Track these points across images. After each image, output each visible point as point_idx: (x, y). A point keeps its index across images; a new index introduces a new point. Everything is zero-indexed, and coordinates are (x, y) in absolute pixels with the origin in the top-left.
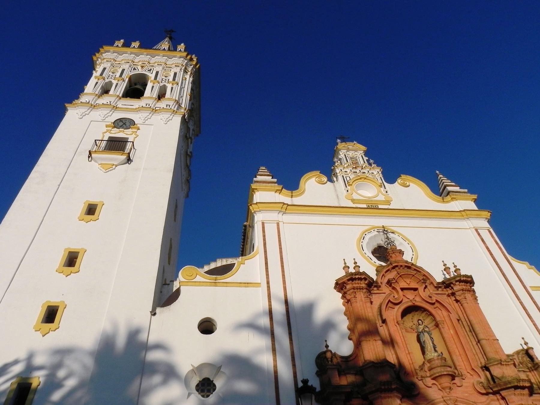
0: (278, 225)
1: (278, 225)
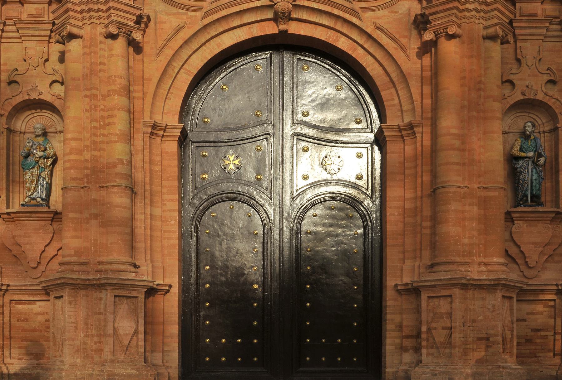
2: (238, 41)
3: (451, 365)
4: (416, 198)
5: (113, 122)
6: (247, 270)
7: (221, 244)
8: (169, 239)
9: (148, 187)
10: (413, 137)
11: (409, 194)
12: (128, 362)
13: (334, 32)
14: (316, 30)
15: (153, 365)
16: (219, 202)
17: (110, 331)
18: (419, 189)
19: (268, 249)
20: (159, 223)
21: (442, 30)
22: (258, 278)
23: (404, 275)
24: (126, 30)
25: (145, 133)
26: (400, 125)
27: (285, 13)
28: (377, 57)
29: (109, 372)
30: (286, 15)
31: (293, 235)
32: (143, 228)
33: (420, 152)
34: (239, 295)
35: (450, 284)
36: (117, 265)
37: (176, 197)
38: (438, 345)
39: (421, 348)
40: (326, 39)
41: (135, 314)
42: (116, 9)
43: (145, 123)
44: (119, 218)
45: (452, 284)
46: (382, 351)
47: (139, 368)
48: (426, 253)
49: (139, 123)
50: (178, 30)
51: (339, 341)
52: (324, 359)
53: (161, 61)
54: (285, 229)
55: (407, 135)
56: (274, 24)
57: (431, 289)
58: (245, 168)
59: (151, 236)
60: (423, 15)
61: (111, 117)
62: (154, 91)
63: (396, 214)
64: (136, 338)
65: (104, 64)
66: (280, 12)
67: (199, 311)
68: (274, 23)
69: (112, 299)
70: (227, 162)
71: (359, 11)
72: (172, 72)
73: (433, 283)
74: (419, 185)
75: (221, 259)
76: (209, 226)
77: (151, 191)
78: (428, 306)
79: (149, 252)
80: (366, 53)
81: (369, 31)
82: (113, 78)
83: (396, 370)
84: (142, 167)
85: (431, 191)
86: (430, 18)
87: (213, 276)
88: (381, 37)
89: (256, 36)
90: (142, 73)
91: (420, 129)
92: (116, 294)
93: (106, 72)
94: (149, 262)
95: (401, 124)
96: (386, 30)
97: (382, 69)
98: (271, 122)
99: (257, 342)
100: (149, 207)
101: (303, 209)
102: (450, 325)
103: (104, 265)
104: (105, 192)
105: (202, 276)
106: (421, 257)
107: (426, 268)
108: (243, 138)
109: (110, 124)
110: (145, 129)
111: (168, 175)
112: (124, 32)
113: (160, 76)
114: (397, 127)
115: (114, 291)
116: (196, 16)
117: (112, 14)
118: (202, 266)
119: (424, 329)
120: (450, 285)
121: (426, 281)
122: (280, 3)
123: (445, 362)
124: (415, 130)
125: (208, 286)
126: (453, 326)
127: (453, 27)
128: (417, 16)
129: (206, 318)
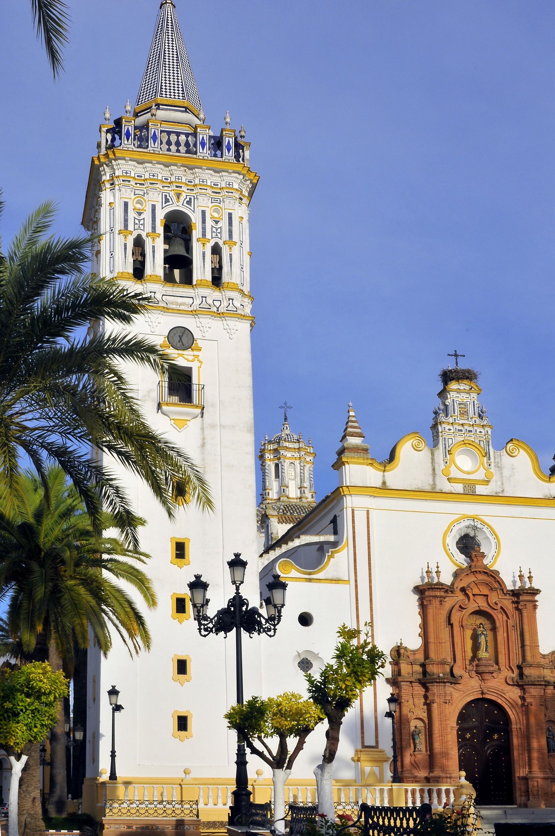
0: (368, 511)
1: (368, 511)
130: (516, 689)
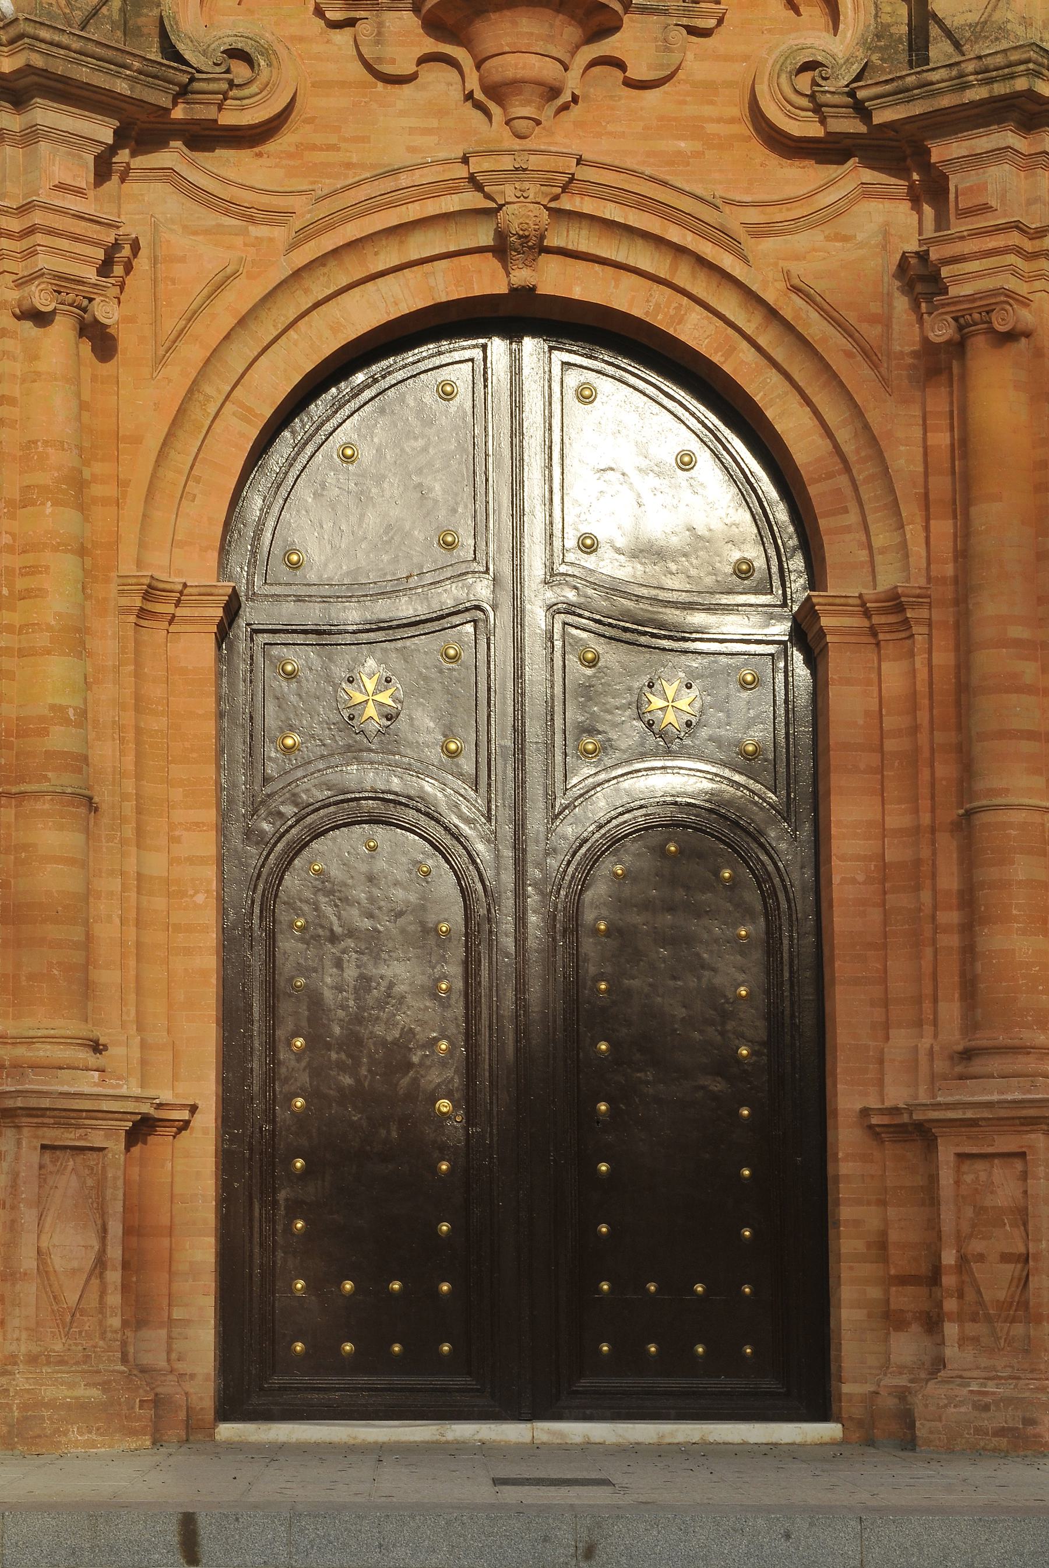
2: (392, 317)
3: (1030, 1376)
4: (916, 830)
5: (39, 590)
6: (420, 1053)
7: (339, 964)
8: (188, 951)
9: (129, 786)
10: (903, 635)
11: (897, 819)
12: (77, 1363)
13: (668, 291)
14: (616, 286)
15: (143, 1371)
16: (333, 829)
17: (28, 1262)
18: (925, 803)
19: (480, 982)
20: (159, 903)
21: (976, 316)
22: (453, 1078)
23: (888, 1079)
24: (77, 295)
25: (125, 611)
26: (866, 597)
27: (527, 237)
28: (796, 377)
29: (27, 1396)
30: (530, 244)
31: (554, 939)
32: (117, 921)
33: (927, 685)
34: (394, 1135)
35: (1019, 1118)
36: (49, 1047)
37: (210, 815)
38: (991, 1312)
39: (943, 1321)
40: (647, 313)
41: (95, 1205)
42: (51, 232)
43: (125, 581)
44: (56, 895)
45: (1025, 1118)
46: (829, 1324)
47: (108, 1382)
48: (951, 1010)
49: (107, 581)
50: (219, 286)
51: (700, 1289)
52: (653, 1349)
53: (170, 381)
54: (533, 919)
55: (886, 629)
56: (497, 265)
57: (963, 1130)
58: (411, 719)
59: (139, 945)
60: (923, 257)
61: (30, 571)
62: (149, 476)
63: (861, 878)
64: (98, 1281)
65: (12, 401)
66: (515, 235)
67: (274, 1188)
68: (496, 261)
69: (35, 1157)
70: (359, 697)
71: (741, 233)
72: (201, 414)
73: (969, 1114)
74: (924, 791)
75: (341, 1013)
76: (306, 908)
77: (138, 796)
78: (957, 1183)
79: (132, 997)
80: (764, 362)
81: (770, 297)
82: (40, 449)
83: (872, 1389)
84: (114, 722)
85: (959, 815)
86: (945, 272)
87: (316, 1072)
88: (805, 316)
89: (444, 299)
90: (114, 419)
91: (924, 613)
92: (45, 1142)
93: (17, 426)
94: (132, 1029)
95: (868, 592)
96: (819, 299)
97: (811, 414)
98: (488, 569)
99: (451, 1292)
100: (133, 849)
101: (585, 854)
102: (1022, 1249)
103: (9, 1046)
104: (13, 812)
105: (283, 1070)
106: (935, 1023)
107: (951, 1058)
108: (405, 621)
109: (27, 595)
110: (124, 601)
111: (187, 745)
112: (70, 301)
113: (166, 430)
114: (857, 601)
115: (40, 1132)
116: (271, 240)
117: (38, 248)
118: (283, 1038)
119: (949, 1258)
120: (1017, 1122)
121: (948, 1106)
122: (515, 206)
123: (1013, 1367)
124: (909, 615)
125: (299, 1102)
126: (1031, 1251)
127: (1006, 311)
128: (907, 257)
129: (295, 1209)
130: (867, 192)
